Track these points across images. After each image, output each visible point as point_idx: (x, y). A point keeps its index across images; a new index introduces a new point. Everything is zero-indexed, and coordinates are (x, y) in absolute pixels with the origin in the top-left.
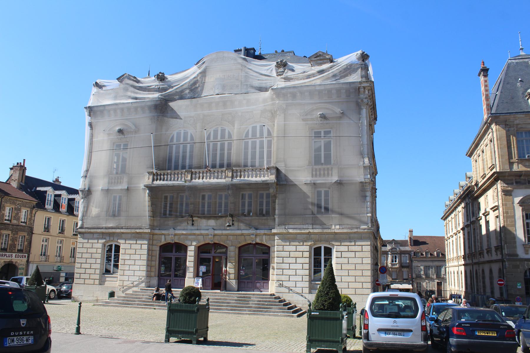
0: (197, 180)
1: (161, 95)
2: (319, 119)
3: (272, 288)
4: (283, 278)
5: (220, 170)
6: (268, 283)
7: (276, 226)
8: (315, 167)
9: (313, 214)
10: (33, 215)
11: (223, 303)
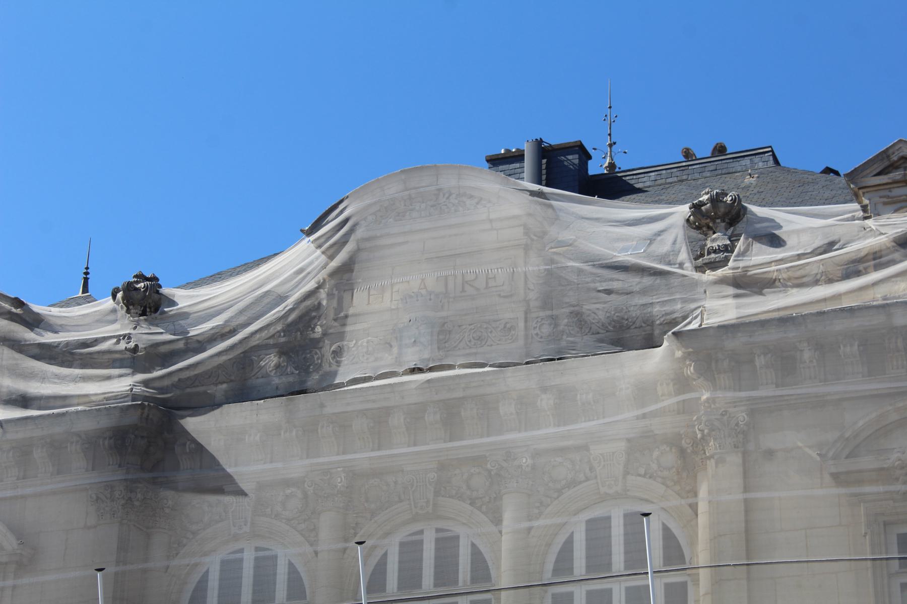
1: (146, 383)
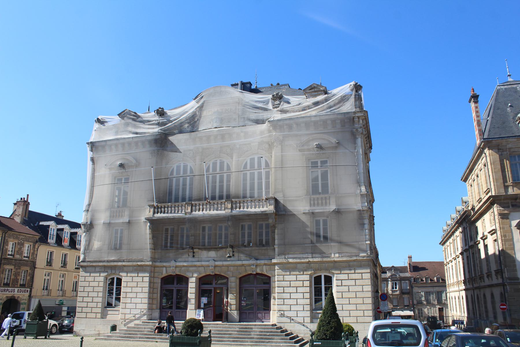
0: (197, 212)
1: (161, 130)
2: (316, 149)
3: (274, 318)
4: (284, 308)
5: (220, 202)
7: (276, 255)
8: (315, 196)
9: (312, 242)
10: (36, 250)
11: (225, 334)
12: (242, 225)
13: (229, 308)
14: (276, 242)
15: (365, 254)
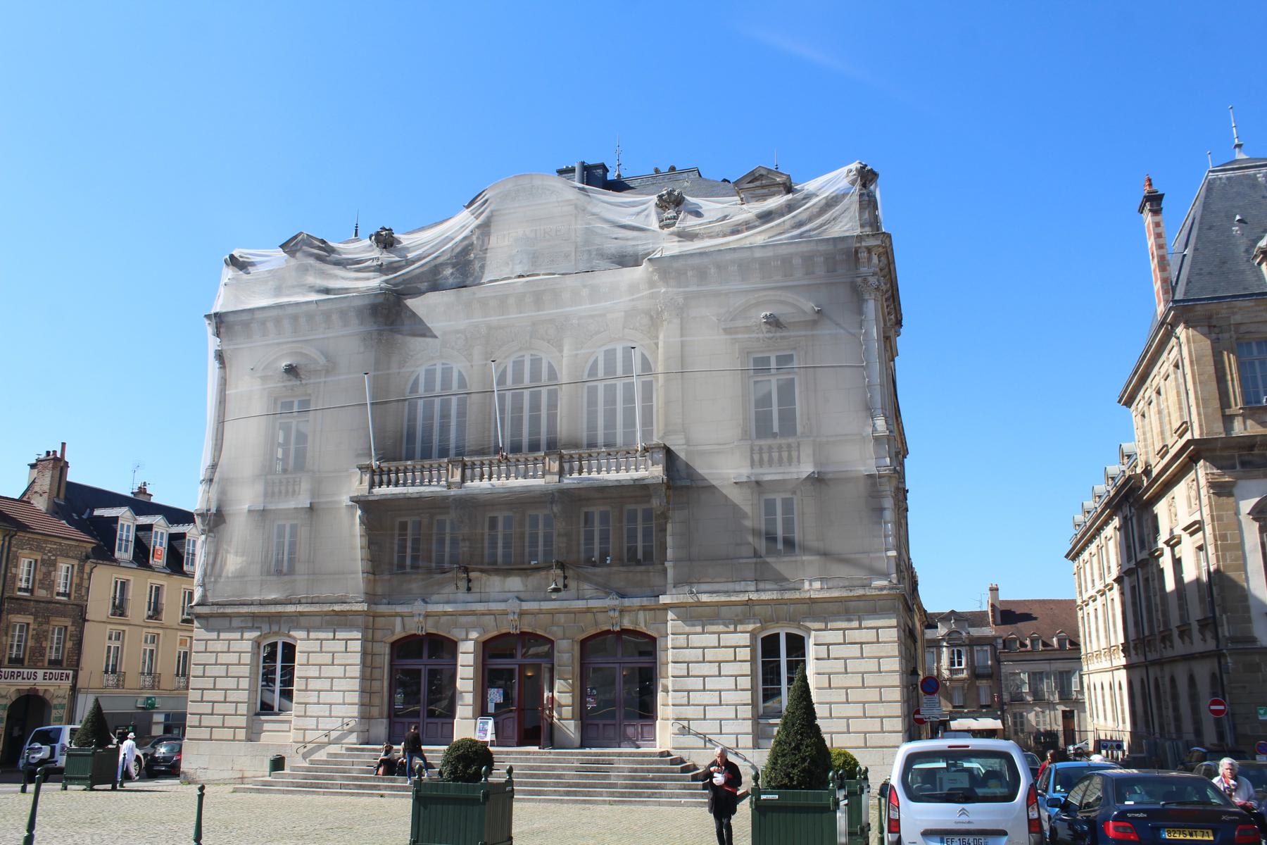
0: (477, 483)
1: (386, 281)
2: (764, 328)
4: (689, 712)
5: (531, 456)
6: (654, 726)
7: (670, 586)
9: (756, 554)
10: (86, 576)
12: (586, 513)
13: (555, 714)
14: (669, 552)
15: (885, 583)
